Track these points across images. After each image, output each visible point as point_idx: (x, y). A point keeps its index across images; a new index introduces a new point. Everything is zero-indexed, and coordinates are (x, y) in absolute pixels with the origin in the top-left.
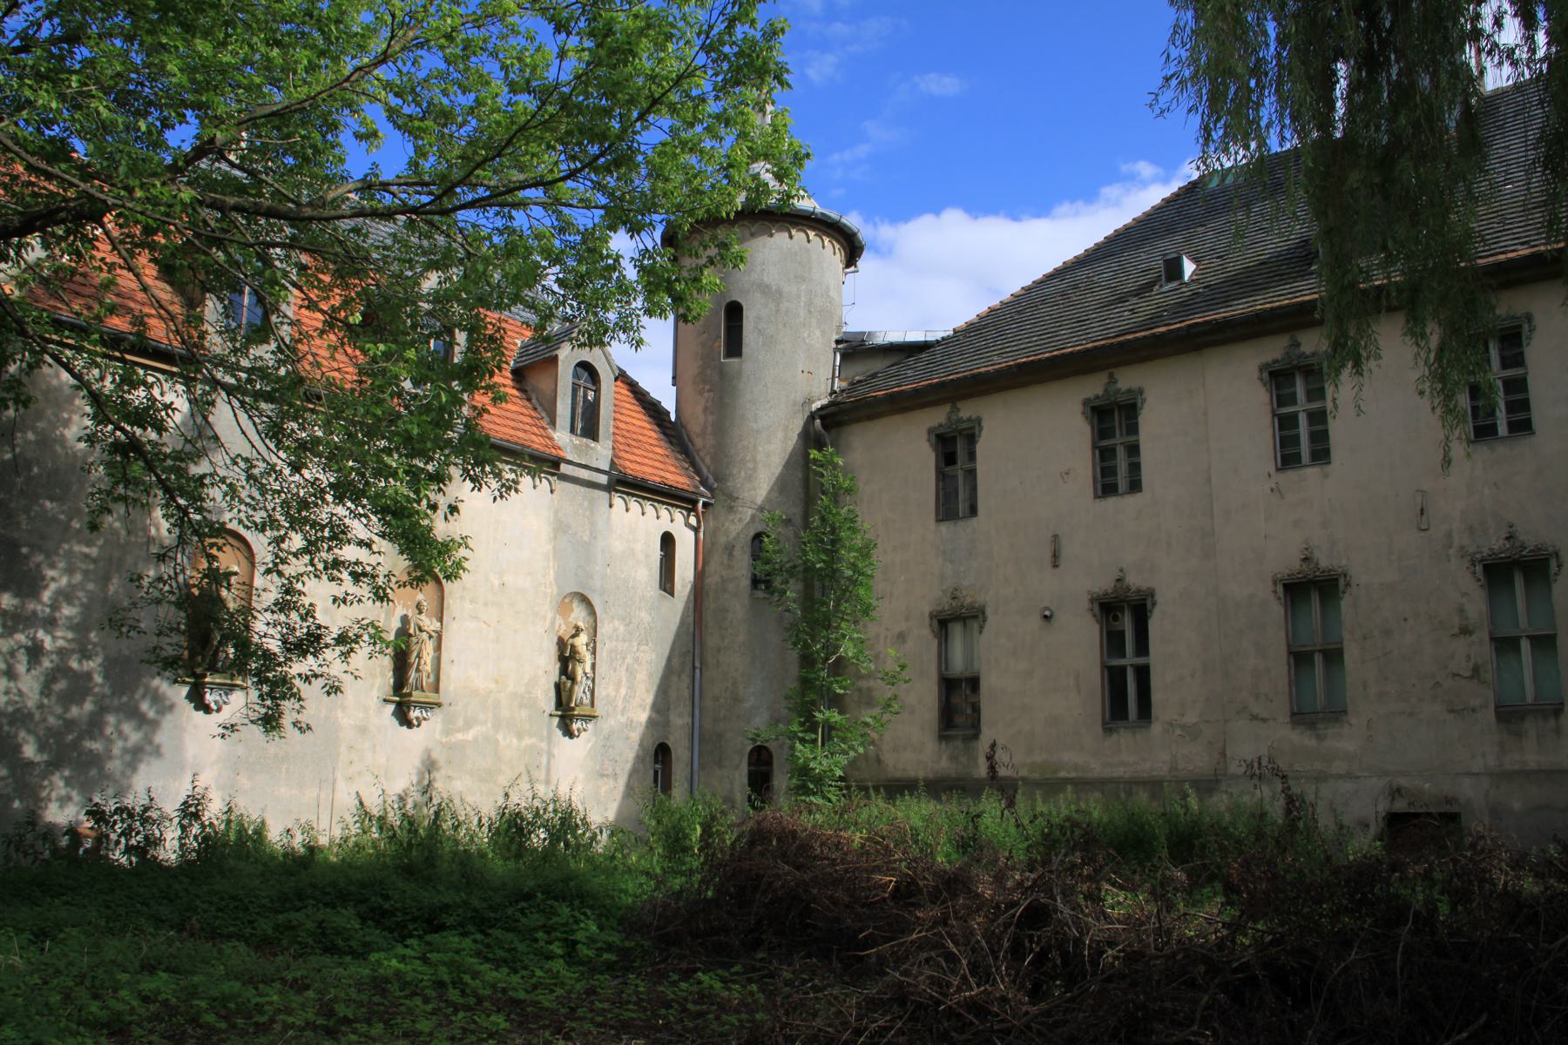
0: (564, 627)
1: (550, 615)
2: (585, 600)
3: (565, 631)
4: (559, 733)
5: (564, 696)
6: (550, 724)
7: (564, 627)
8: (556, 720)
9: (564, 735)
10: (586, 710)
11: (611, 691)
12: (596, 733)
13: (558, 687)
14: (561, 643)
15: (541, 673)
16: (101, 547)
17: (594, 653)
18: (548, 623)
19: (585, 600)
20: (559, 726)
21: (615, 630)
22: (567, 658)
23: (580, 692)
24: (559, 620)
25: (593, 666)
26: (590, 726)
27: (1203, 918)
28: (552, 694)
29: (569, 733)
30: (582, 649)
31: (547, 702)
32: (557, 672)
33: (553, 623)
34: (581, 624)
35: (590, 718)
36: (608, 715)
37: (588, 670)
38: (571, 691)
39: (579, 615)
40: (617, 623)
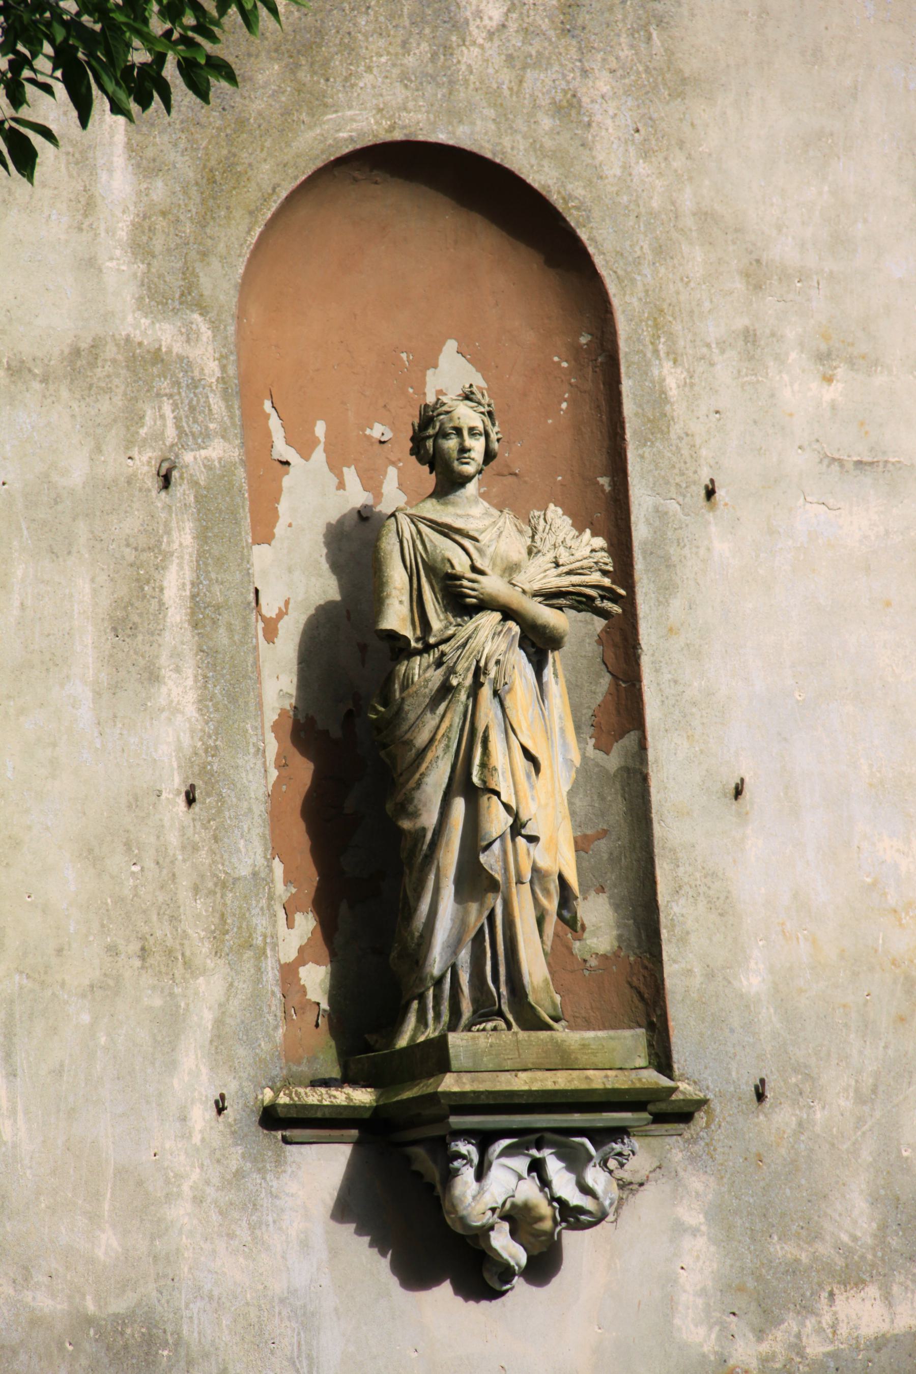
9: (416, 1273)
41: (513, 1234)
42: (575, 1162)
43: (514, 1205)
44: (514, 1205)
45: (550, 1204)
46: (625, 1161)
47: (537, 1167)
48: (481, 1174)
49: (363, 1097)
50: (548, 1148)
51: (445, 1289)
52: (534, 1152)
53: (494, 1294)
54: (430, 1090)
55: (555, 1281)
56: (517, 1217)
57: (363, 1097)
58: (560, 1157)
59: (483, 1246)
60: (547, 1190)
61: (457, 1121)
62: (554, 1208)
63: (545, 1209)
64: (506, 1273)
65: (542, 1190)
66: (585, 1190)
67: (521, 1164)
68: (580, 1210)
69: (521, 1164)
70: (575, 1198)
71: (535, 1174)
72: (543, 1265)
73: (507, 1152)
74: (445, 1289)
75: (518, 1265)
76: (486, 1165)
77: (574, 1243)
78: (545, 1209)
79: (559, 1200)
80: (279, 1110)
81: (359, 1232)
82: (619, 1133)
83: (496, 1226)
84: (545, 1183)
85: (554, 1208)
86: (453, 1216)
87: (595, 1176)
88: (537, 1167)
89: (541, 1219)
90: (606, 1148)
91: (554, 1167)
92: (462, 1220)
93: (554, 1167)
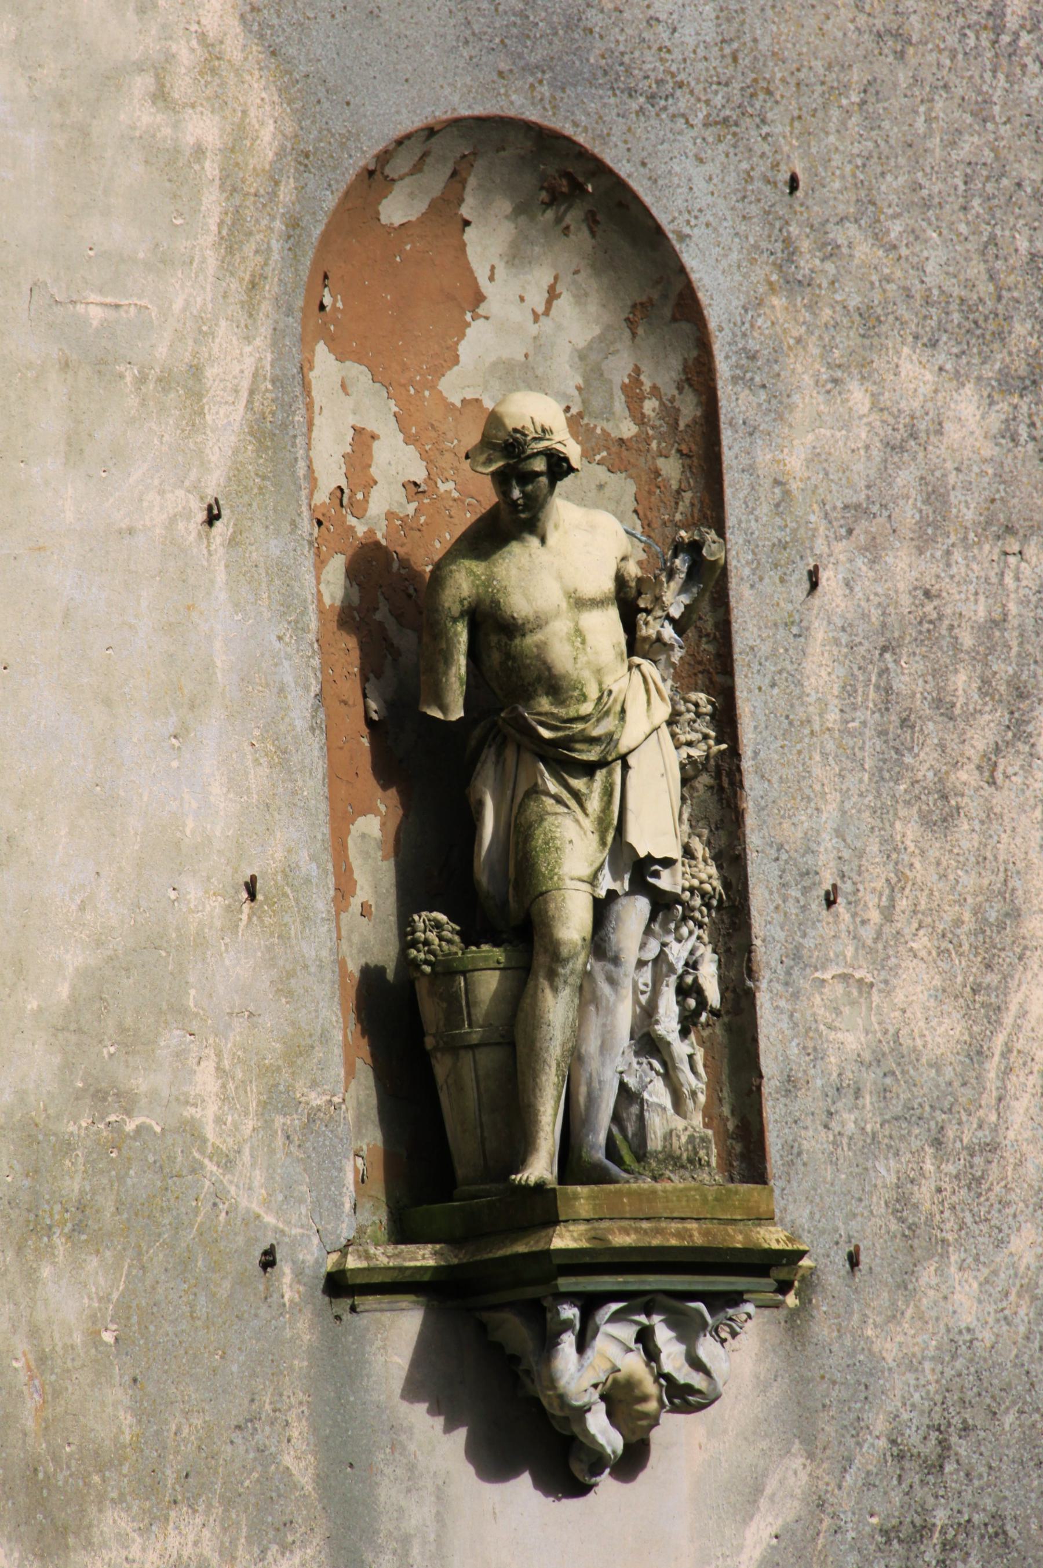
0: (396, 461)
1: (238, 360)
2: (574, 191)
3: (406, 484)
4: (437, 1446)
5: (462, 1087)
6: (339, 1372)
7: (396, 461)
8: (397, 1332)
9: (495, 1459)
10: (674, 1207)
11: (921, 1010)
12: (803, 1417)
13: (394, 1015)
14: (390, 613)
15: (204, 901)
16: (648, 1315)
17: (711, 669)
18: (226, 420)
19: (574, 191)
20: (437, 1380)
21: (907, 436)
22: (444, 722)
23: (603, 1035)
24: (344, 400)
25: (717, 791)
26: (740, 1356)
27: (688, 496)
28: (341, 1087)
29: (539, 1444)
30: (588, 648)
31: (290, 1154)
32: (374, 878)
33: (279, 424)
34: (538, 412)
35: (717, 1278)
36: (918, 1239)
37: (657, 823)
38: (514, 1037)
39: (531, 344)
40: (913, 374)
41: (610, 1414)
42: (687, 1330)
43: (615, 1382)
44: (615, 1382)
45: (656, 1381)
46: (738, 1329)
47: (645, 1337)
48: (582, 1346)
49: (423, 1257)
50: (658, 1314)
51: (524, 1481)
52: (642, 1319)
53: (579, 1489)
54: (541, 1246)
55: (643, 1476)
56: (618, 1397)
57: (423, 1257)
58: (671, 1324)
59: (576, 1429)
60: (653, 1364)
61: (565, 1284)
62: (661, 1386)
63: (650, 1387)
64: (597, 1462)
65: (648, 1365)
66: (696, 1364)
67: (627, 1332)
68: (689, 1389)
69: (627, 1332)
70: (684, 1375)
71: (640, 1346)
72: (633, 1460)
73: (616, 1317)
74: (524, 1481)
75: (614, 1452)
76: (589, 1333)
77: (673, 1432)
78: (650, 1387)
79: (668, 1377)
80: (348, 1274)
81: (433, 1412)
82: (735, 1299)
83: (594, 1408)
84: (652, 1355)
85: (661, 1386)
86: (550, 1393)
87: (707, 1348)
88: (645, 1337)
89: (645, 1398)
90: (721, 1316)
91: (664, 1336)
92: (562, 1398)
93: (664, 1336)
